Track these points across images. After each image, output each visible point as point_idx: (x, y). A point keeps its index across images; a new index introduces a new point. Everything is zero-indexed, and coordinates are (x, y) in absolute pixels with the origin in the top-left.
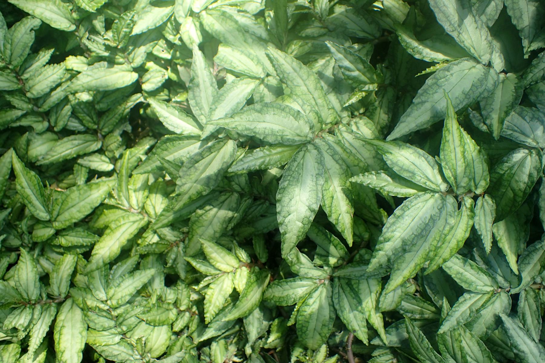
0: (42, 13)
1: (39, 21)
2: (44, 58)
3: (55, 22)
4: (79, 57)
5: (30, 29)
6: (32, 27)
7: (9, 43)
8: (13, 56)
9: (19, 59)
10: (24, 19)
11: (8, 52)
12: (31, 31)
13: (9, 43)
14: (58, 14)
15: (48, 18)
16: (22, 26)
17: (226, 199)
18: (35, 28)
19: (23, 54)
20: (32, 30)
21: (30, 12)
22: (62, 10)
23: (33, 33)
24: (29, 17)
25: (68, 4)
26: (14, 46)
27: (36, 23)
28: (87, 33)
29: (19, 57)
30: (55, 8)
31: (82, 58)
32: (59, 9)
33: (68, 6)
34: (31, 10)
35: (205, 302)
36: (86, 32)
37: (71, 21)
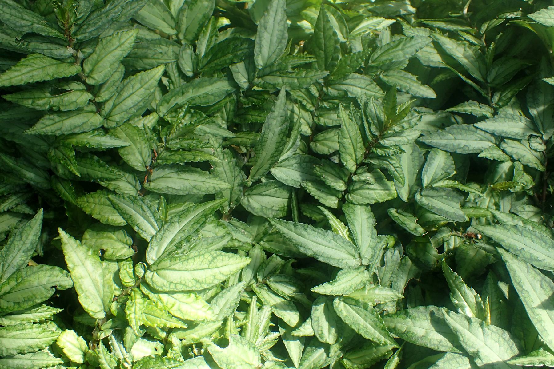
0: (81, 278)
1: (71, 283)
2: (43, 314)
3: (87, 297)
4: (81, 338)
5: (53, 285)
6: (58, 284)
7: (17, 281)
8: (8, 295)
9: (12, 304)
10: (57, 268)
11: (7, 288)
12: (52, 288)
13: (17, 281)
14: (98, 291)
15: (83, 287)
16: (48, 273)
17: (163, 254)
18: (59, 288)
19: (21, 304)
20: (55, 287)
21: (70, 265)
22: (106, 289)
23: (52, 292)
24: (65, 271)
25: (117, 287)
26: (19, 287)
27: (66, 283)
28: (112, 331)
29: (14, 303)
30: (100, 281)
31: (84, 342)
32: (104, 286)
33: (115, 289)
34: (74, 264)
35: (138, 74)
36: (110, 328)
37: (104, 307)
